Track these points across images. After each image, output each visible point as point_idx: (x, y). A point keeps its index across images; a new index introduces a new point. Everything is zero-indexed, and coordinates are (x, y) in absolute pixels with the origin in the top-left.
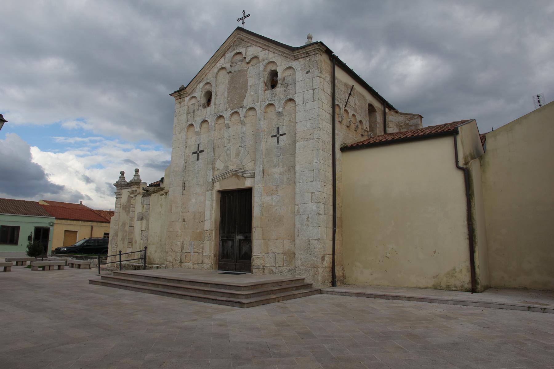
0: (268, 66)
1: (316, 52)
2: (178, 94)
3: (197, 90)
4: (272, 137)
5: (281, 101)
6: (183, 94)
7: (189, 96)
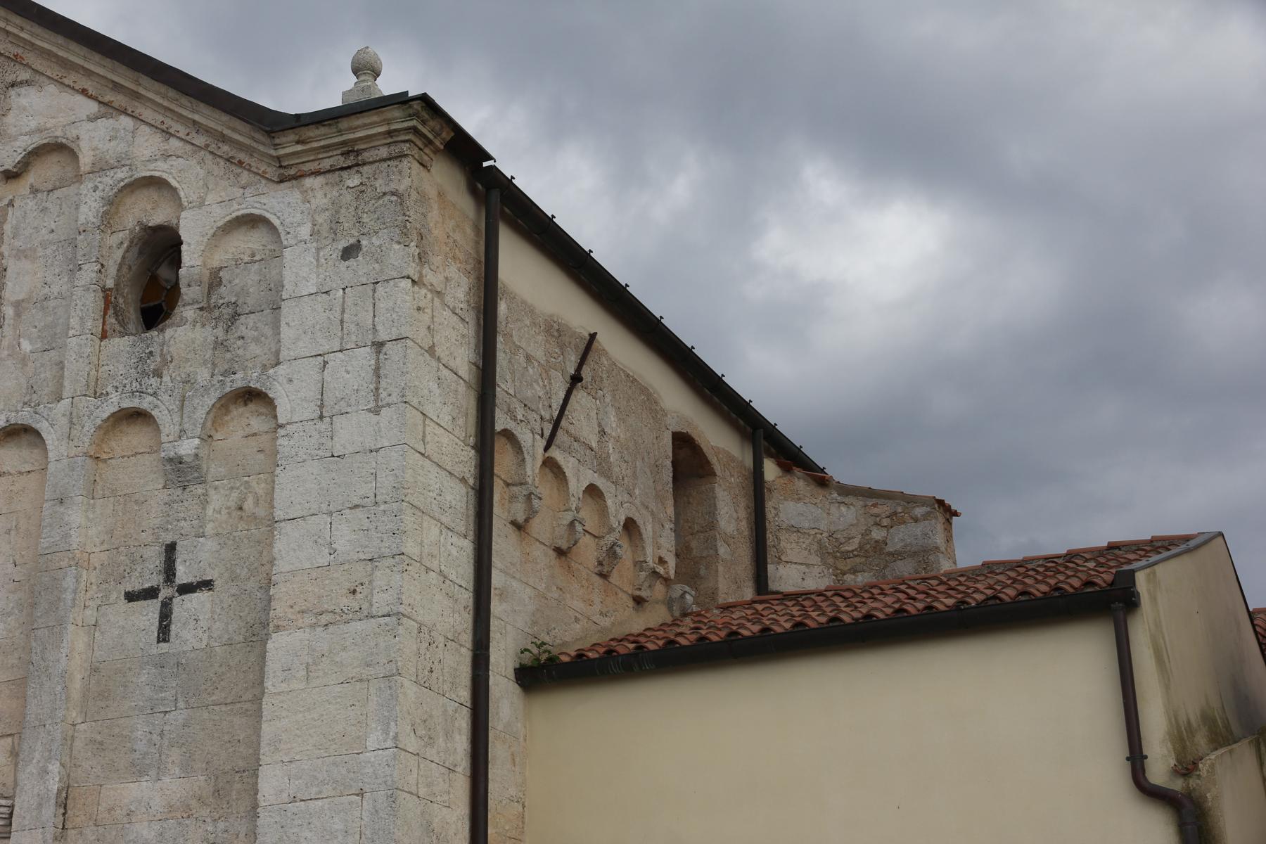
0: (129, 201)
1: (395, 150)
4: (131, 597)
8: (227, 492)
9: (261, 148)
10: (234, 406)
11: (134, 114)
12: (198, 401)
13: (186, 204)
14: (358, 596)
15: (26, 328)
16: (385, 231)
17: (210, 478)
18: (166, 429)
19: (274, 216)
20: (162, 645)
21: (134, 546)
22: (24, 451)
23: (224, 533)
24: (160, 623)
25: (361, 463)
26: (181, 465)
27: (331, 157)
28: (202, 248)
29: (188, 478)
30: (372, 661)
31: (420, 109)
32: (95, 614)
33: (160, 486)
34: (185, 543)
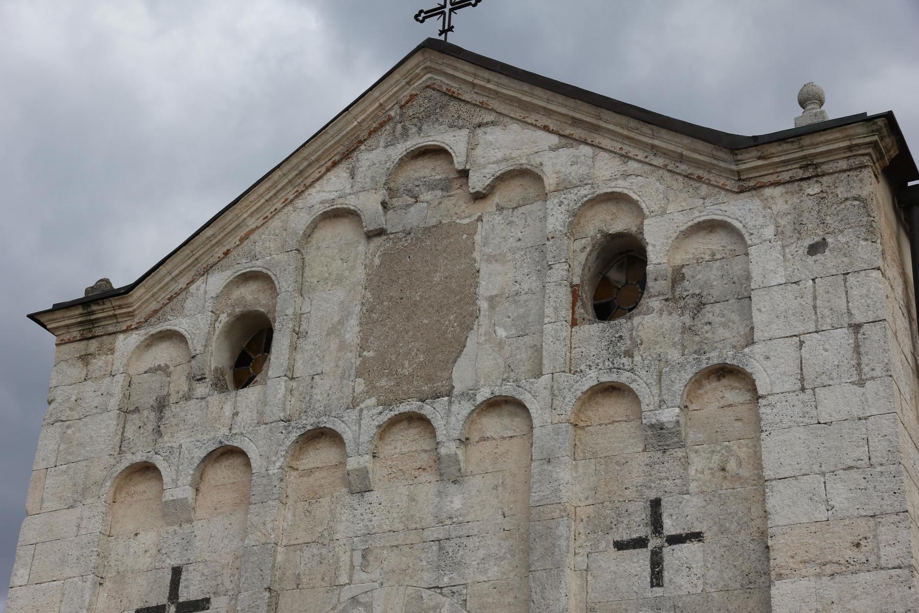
0: (590, 214)
1: (856, 162)
2: (82, 315)
3: (189, 304)
4: (620, 546)
5: (673, 376)
6: (105, 318)
7: (142, 332)
8: (708, 455)
9: (722, 164)
10: (707, 381)
11: (594, 143)
12: (676, 376)
13: (648, 213)
14: (863, 549)
15: (500, 318)
16: (851, 230)
17: (689, 443)
18: (646, 400)
19: (735, 221)
20: (655, 589)
21: (619, 501)
22: (505, 420)
23: (709, 490)
24: (652, 569)
25: (850, 429)
26: (662, 431)
27: (789, 170)
28: (667, 248)
29: (668, 443)
30: (887, 609)
31: (883, 126)
32: (586, 560)
33: (640, 450)
34: (670, 499)
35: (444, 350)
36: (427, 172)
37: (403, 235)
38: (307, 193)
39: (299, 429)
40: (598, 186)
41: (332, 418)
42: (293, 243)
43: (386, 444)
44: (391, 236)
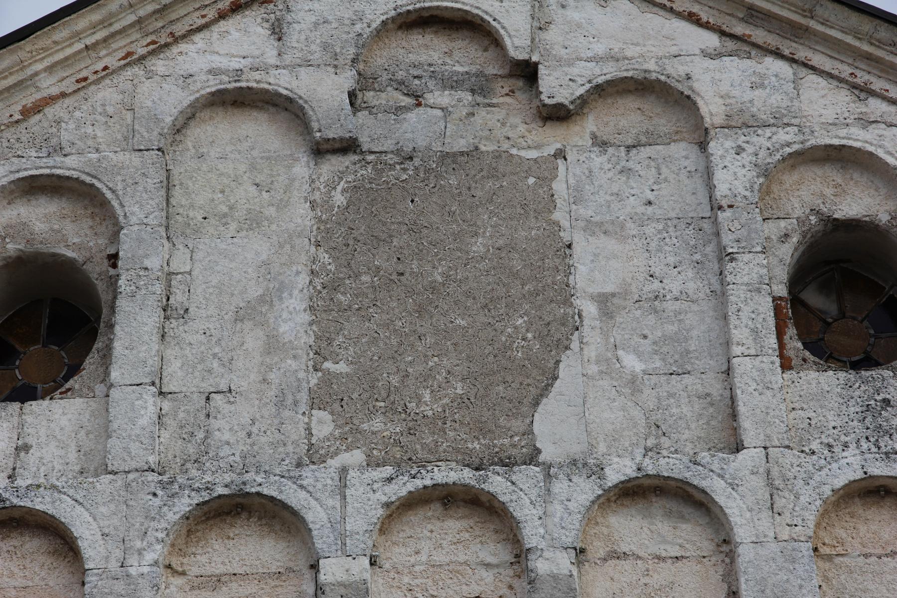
0: (790, 179)
35: (509, 378)
36: (435, 56)
37: (396, 159)
38: (175, 50)
39: (198, 490)
40: (813, 132)
41: (277, 478)
42: (150, 136)
43: (394, 543)
44: (370, 158)
